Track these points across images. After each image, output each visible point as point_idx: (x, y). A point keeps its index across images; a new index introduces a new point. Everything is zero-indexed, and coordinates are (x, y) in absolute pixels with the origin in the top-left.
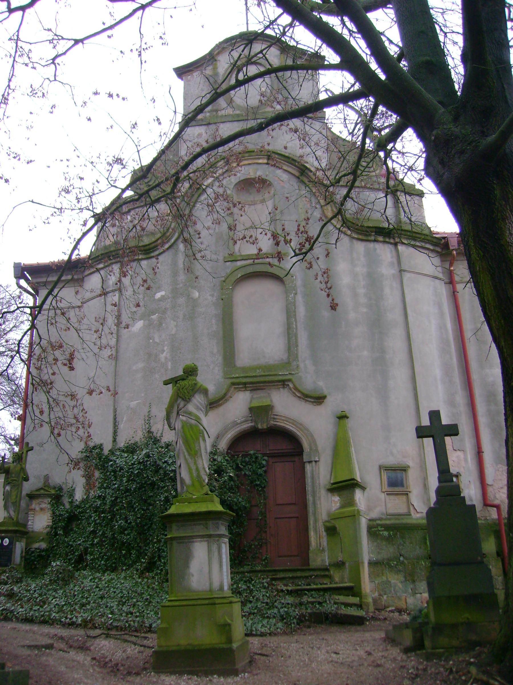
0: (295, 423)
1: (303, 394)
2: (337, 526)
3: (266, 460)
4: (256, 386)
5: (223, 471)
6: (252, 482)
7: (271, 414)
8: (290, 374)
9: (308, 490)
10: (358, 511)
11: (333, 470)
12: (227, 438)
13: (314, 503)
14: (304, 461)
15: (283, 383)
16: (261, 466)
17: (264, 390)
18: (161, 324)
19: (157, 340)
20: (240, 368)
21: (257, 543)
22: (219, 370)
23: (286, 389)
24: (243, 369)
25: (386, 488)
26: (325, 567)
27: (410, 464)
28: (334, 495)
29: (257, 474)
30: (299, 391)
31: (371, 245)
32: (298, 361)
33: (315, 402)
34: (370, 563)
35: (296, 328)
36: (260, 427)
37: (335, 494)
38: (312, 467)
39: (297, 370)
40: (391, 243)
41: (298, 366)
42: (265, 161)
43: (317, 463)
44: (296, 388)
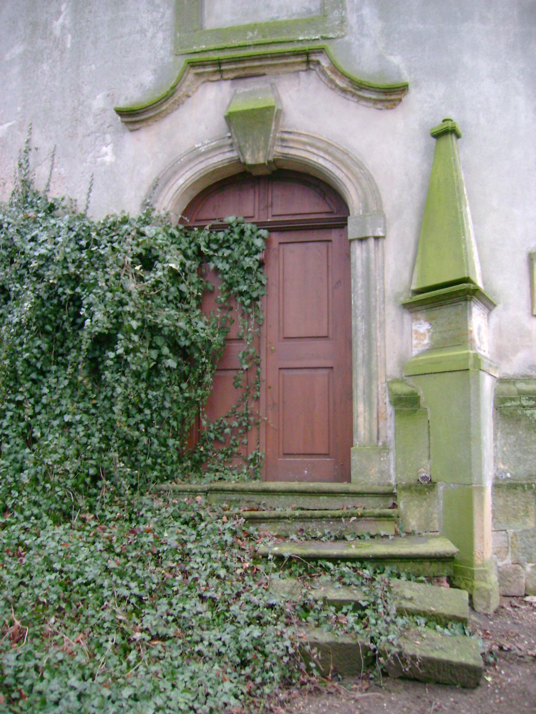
0: (330, 150)
1: (352, 81)
2: (421, 393)
3: (263, 238)
4: (244, 69)
5: (156, 258)
6: (230, 286)
7: (276, 130)
8: (324, 38)
9: (356, 307)
10: (477, 359)
11: (419, 257)
12: (175, 187)
13: (369, 337)
14: (350, 237)
16: (252, 251)
17: (264, 78)
20: (211, 31)
21: (235, 424)
22: (164, 39)
23: (313, 74)
24: (218, 33)
26: (386, 489)
28: (417, 319)
29: (242, 269)
30: (343, 75)
32: (344, 8)
33: (381, 101)
34: (497, 486)
36: (249, 160)
37: (419, 316)
38: (368, 252)
39: (341, 30)
41: (343, 21)
43: (380, 243)
44: (335, 69)
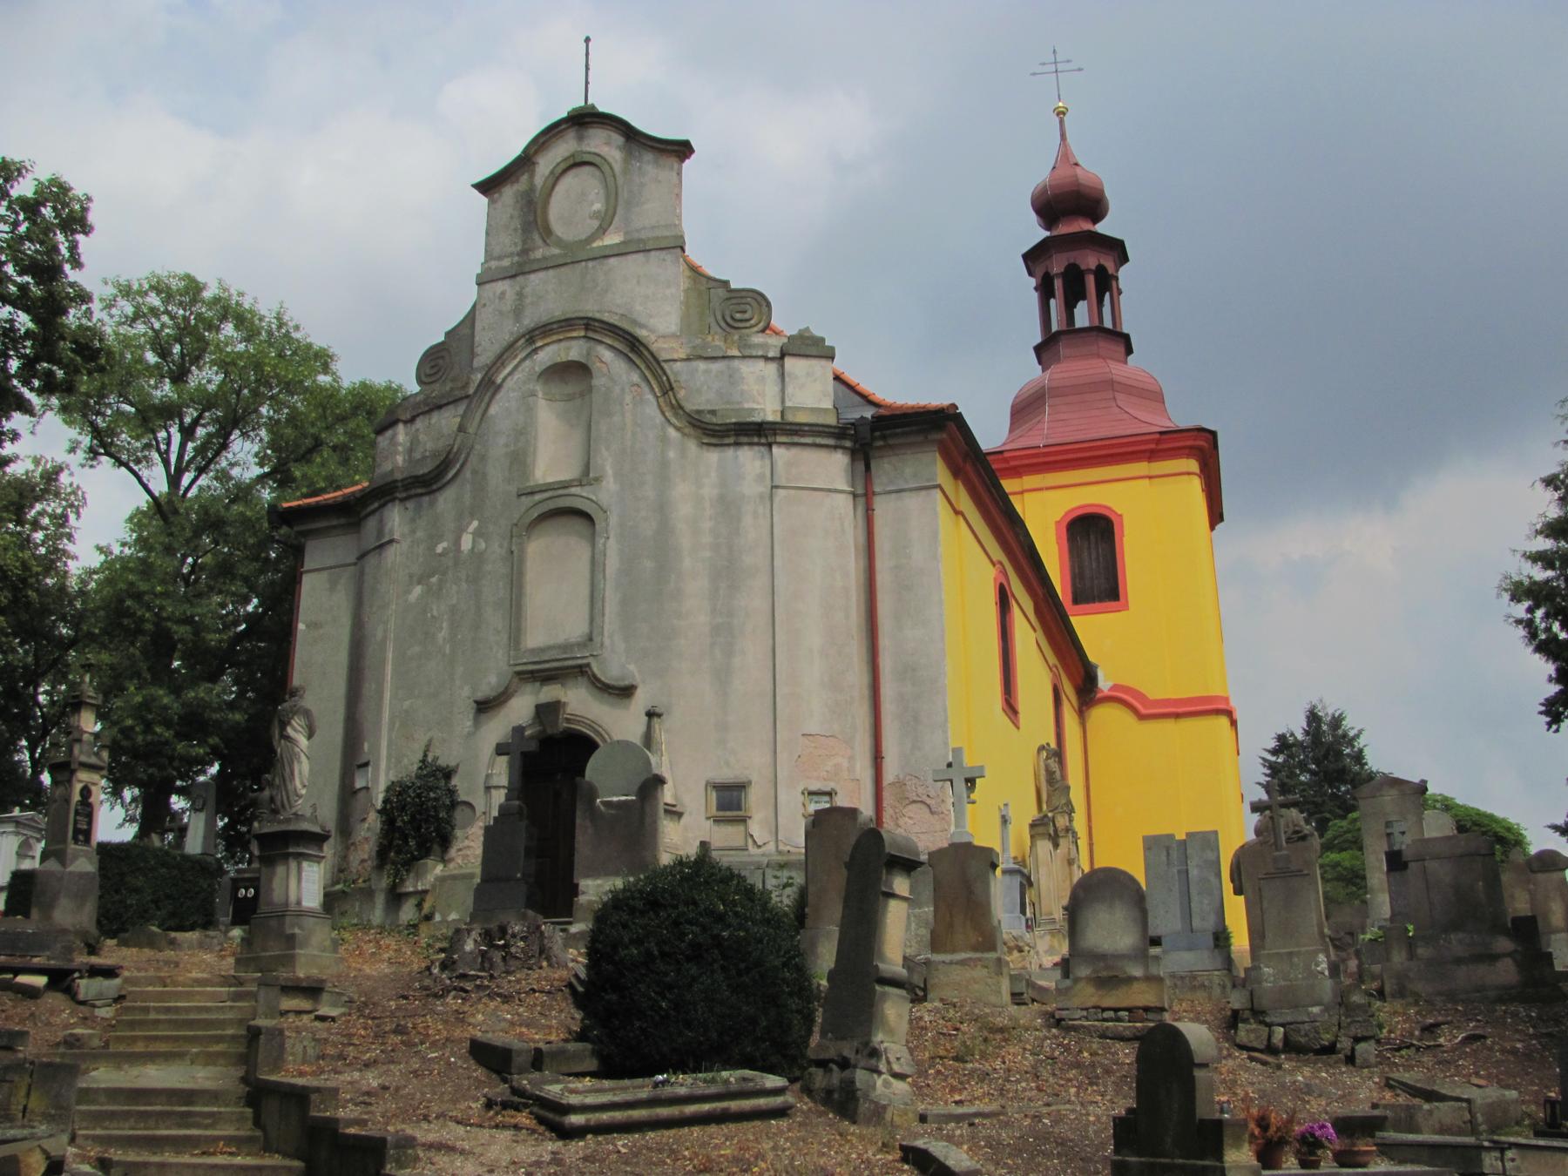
15: (582, 671)
18: (440, 589)
19: (435, 613)
25: (714, 811)
27: (754, 778)
31: (730, 452)
35: (604, 590)
40: (763, 445)
41: (602, 645)
42: (582, 333)
